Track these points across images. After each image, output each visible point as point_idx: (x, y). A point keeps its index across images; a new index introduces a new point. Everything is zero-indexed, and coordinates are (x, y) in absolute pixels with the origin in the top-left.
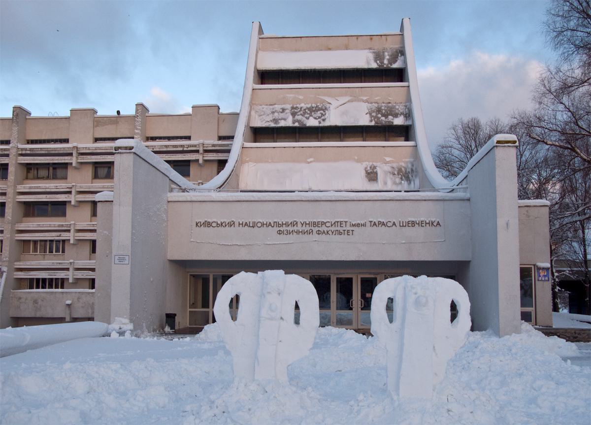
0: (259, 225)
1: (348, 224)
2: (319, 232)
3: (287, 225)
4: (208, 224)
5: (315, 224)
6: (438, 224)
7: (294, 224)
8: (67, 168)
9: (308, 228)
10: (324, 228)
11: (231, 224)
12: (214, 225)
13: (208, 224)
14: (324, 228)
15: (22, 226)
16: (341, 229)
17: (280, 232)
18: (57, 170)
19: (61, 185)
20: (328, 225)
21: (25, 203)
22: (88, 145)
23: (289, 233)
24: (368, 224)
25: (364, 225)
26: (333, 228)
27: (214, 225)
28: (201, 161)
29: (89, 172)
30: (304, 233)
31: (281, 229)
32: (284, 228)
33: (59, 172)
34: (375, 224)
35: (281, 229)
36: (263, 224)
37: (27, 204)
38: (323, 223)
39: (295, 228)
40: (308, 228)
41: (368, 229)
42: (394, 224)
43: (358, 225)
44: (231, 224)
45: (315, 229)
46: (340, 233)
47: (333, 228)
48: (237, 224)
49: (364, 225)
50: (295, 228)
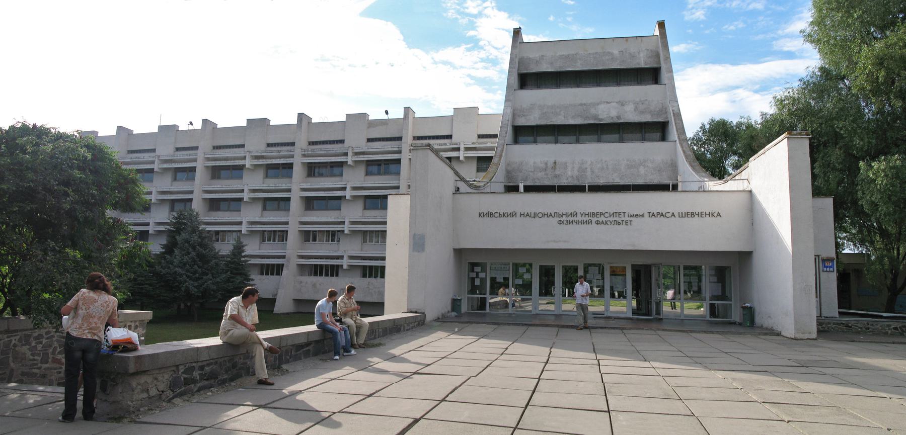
0: (540, 215)
1: (626, 215)
2: (598, 223)
3: (567, 215)
4: (491, 215)
5: (594, 215)
6: (719, 214)
7: (574, 214)
8: (342, 166)
9: (587, 218)
10: (602, 219)
11: (513, 215)
12: (497, 215)
13: (491, 215)
14: (602, 219)
15: (305, 219)
16: (620, 220)
17: (560, 222)
18: (335, 168)
19: (234, 184)
20: (606, 215)
21: (307, 197)
22: (363, 146)
23: (569, 223)
24: (647, 215)
25: (643, 216)
26: (612, 219)
27: (497, 215)
28: (462, 158)
29: (362, 170)
30: (583, 222)
31: (562, 219)
32: (564, 218)
33: (336, 170)
34: (653, 214)
35: (562, 219)
36: (544, 215)
37: (212, 200)
38: (602, 214)
39: (575, 219)
40: (587, 218)
41: (677, 219)
42: (673, 215)
43: (637, 216)
44: (513, 215)
45: (594, 220)
46: (618, 223)
47: (612, 219)
48: (518, 215)
49: (643, 216)
50: (575, 219)
